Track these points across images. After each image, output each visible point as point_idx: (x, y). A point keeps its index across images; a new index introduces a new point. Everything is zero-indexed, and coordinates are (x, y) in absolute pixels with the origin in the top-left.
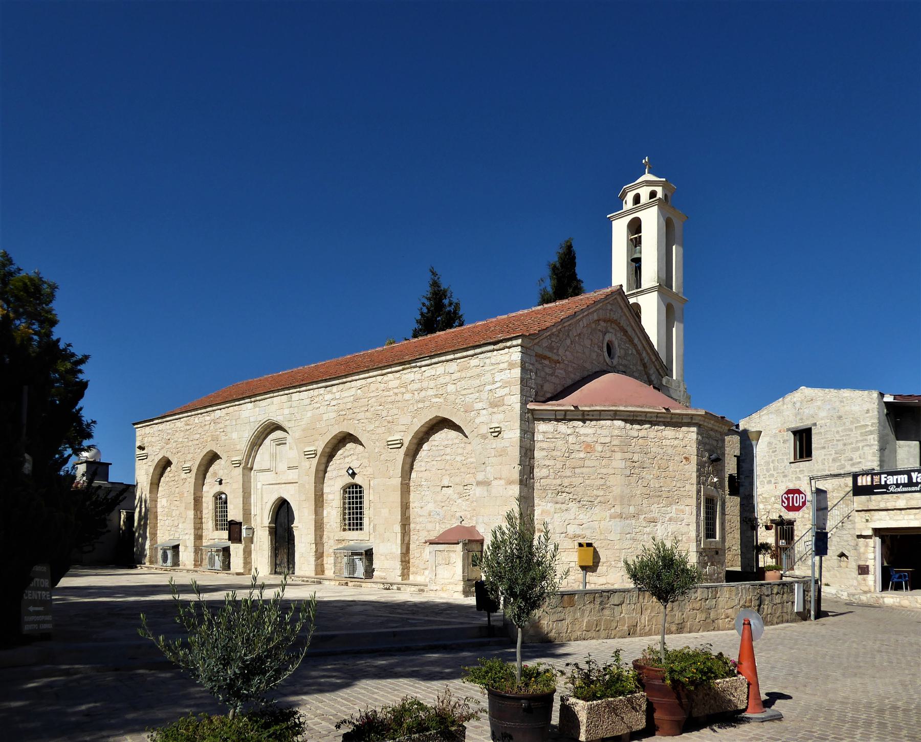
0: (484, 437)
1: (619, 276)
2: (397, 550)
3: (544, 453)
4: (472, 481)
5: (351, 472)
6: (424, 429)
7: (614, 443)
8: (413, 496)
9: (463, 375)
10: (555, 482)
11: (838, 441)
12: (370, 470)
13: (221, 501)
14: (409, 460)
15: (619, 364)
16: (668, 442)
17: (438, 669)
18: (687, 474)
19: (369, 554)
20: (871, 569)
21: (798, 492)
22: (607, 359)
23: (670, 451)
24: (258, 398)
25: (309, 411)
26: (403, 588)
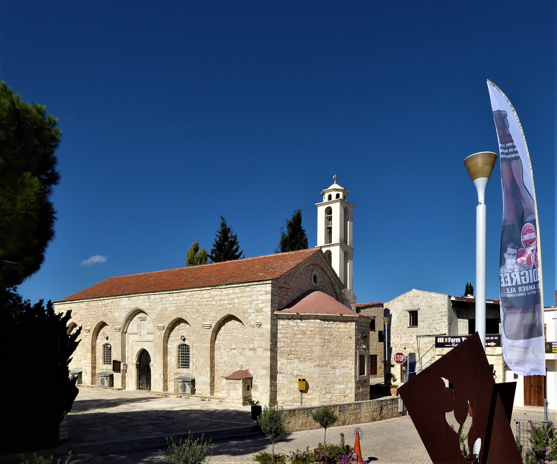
0: (253, 326)
1: (321, 240)
2: (208, 380)
3: (282, 335)
4: (246, 347)
5: (183, 338)
7: (316, 330)
8: (216, 353)
9: (243, 295)
10: (287, 349)
13: (107, 349)
14: (214, 334)
15: (320, 285)
16: (341, 330)
19: (193, 382)
22: (314, 284)
25: (161, 305)
26: (211, 400)
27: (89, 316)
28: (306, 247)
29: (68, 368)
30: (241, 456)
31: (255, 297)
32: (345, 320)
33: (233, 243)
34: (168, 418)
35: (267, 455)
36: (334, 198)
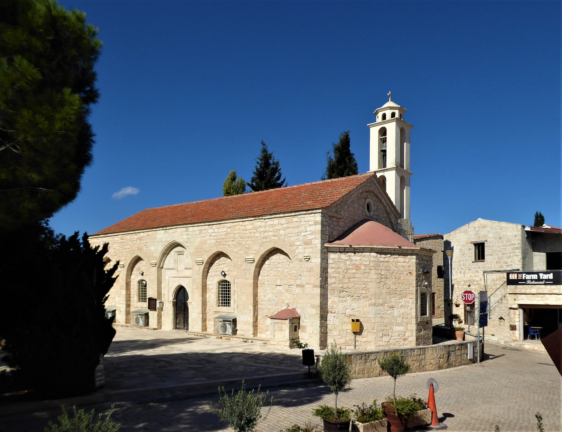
0: (301, 260)
1: (374, 165)
2: (251, 320)
3: (333, 270)
4: (293, 283)
5: (223, 273)
6: (267, 253)
7: (371, 265)
8: (259, 290)
9: (289, 226)
11: (499, 251)
12: (235, 273)
13: (143, 286)
14: (258, 269)
15: (374, 215)
16: (400, 264)
17: (289, 400)
18: (411, 282)
19: (234, 321)
20: (518, 327)
21: (471, 292)
22: (367, 213)
23: (401, 269)
24: (167, 228)
25: (200, 238)
26: (254, 341)
27: (124, 250)
28: (355, 173)
29: (104, 306)
30: (295, 408)
31: (303, 228)
32: (404, 253)
33: (275, 170)
34: (209, 362)
35: (328, 408)
36: (388, 117)
